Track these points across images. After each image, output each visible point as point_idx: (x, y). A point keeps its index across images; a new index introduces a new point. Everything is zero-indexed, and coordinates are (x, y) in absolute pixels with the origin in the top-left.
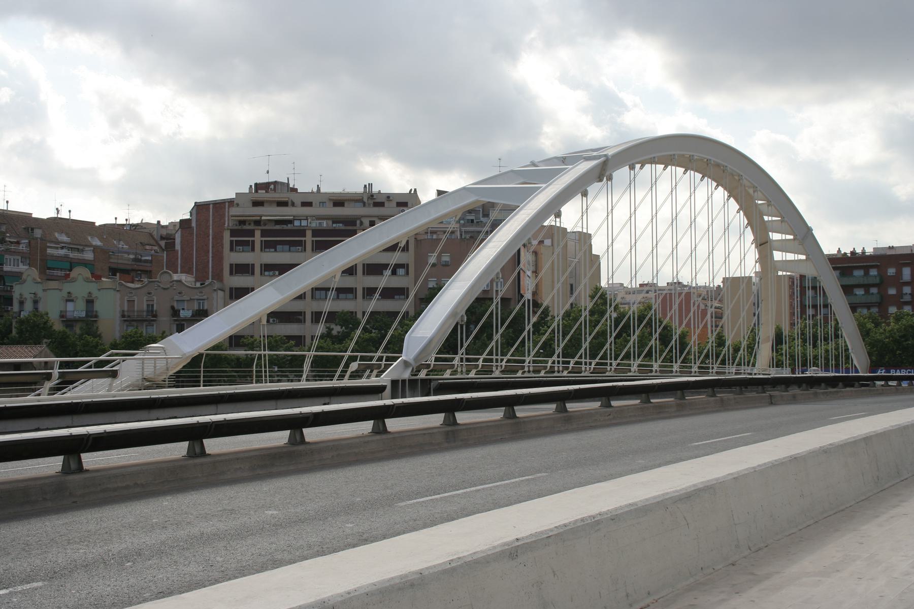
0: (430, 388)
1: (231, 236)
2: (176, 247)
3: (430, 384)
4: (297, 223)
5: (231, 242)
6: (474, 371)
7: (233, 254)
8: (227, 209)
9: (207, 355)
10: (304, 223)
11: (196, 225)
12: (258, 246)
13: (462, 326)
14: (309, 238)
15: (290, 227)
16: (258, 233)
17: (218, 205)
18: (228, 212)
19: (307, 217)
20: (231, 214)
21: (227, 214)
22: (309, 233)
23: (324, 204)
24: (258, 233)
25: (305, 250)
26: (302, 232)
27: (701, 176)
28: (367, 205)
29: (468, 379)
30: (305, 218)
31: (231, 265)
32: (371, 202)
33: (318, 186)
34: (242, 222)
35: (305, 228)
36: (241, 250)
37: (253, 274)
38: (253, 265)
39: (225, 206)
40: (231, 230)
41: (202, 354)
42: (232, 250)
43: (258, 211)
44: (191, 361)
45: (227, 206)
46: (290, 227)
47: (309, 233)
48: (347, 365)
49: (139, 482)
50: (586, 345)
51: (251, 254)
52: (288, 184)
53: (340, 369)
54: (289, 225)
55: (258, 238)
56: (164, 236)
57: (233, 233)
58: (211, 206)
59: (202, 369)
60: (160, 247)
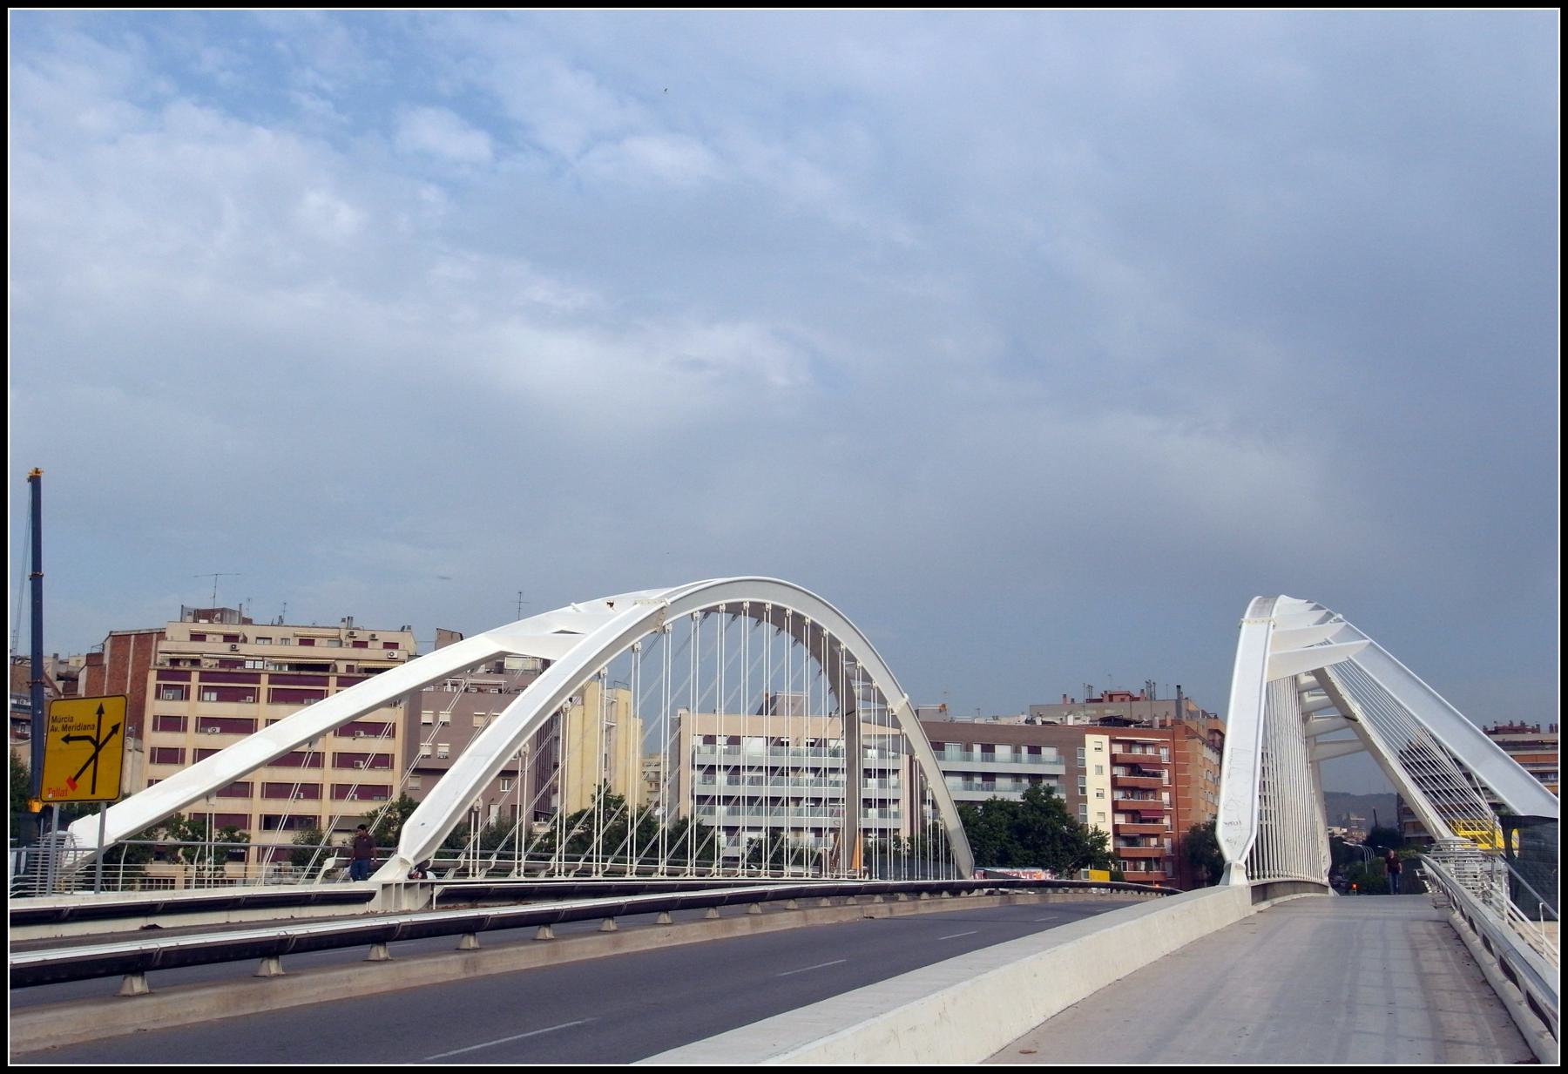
0: (432, 896)
1: (158, 679)
2: (79, 690)
3: (432, 890)
4: (249, 665)
5: (158, 686)
6: (572, 873)
7: (158, 703)
8: (154, 643)
9: (130, 846)
10: (259, 665)
11: (110, 662)
12: (263, 695)
13: (477, 813)
14: (264, 685)
15: (239, 669)
16: (195, 676)
17: (142, 637)
18: (156, 647)
19: (263, 657)
20: (159, 649)
21: (153, 648)
22: (265, 679)
23: (288, 642)
24: (195, 676)
25: (258, 701)
26: (254, 677)
27: (777, 628)
28: (344, 644)
29: (567, 881)
30: (261, 659)
31: (155, 718)
32: (350, 641)
33: (280, 617)
34: (175, 662)
35: (260, 672)
36: (171, 698)
37: (185, 729)
38: (186, 718)
39: (152, 638)
40: (158, 670)
41: (124, 845)
42: (158, 696)
43: (198, 646)
44: (1333, 862)
45: (155, 639)
46: (239, 669)
47: (265, 679)
48: (320, 862)
49: (53, 1034)
50: (598, 839)
51: (254, 706)
52: (240, 613)
53: (309, 867)
54: (238, 668)
55: (195, 681)
56: (61, 675)
57: (162, 675)
58: (133, 637)
59: (122, 865)
60: (56, 690)
